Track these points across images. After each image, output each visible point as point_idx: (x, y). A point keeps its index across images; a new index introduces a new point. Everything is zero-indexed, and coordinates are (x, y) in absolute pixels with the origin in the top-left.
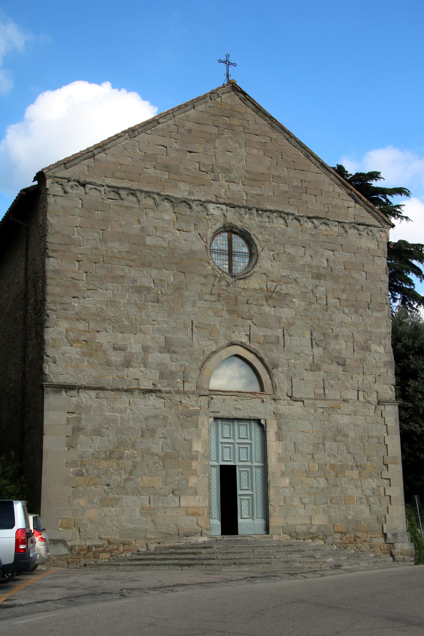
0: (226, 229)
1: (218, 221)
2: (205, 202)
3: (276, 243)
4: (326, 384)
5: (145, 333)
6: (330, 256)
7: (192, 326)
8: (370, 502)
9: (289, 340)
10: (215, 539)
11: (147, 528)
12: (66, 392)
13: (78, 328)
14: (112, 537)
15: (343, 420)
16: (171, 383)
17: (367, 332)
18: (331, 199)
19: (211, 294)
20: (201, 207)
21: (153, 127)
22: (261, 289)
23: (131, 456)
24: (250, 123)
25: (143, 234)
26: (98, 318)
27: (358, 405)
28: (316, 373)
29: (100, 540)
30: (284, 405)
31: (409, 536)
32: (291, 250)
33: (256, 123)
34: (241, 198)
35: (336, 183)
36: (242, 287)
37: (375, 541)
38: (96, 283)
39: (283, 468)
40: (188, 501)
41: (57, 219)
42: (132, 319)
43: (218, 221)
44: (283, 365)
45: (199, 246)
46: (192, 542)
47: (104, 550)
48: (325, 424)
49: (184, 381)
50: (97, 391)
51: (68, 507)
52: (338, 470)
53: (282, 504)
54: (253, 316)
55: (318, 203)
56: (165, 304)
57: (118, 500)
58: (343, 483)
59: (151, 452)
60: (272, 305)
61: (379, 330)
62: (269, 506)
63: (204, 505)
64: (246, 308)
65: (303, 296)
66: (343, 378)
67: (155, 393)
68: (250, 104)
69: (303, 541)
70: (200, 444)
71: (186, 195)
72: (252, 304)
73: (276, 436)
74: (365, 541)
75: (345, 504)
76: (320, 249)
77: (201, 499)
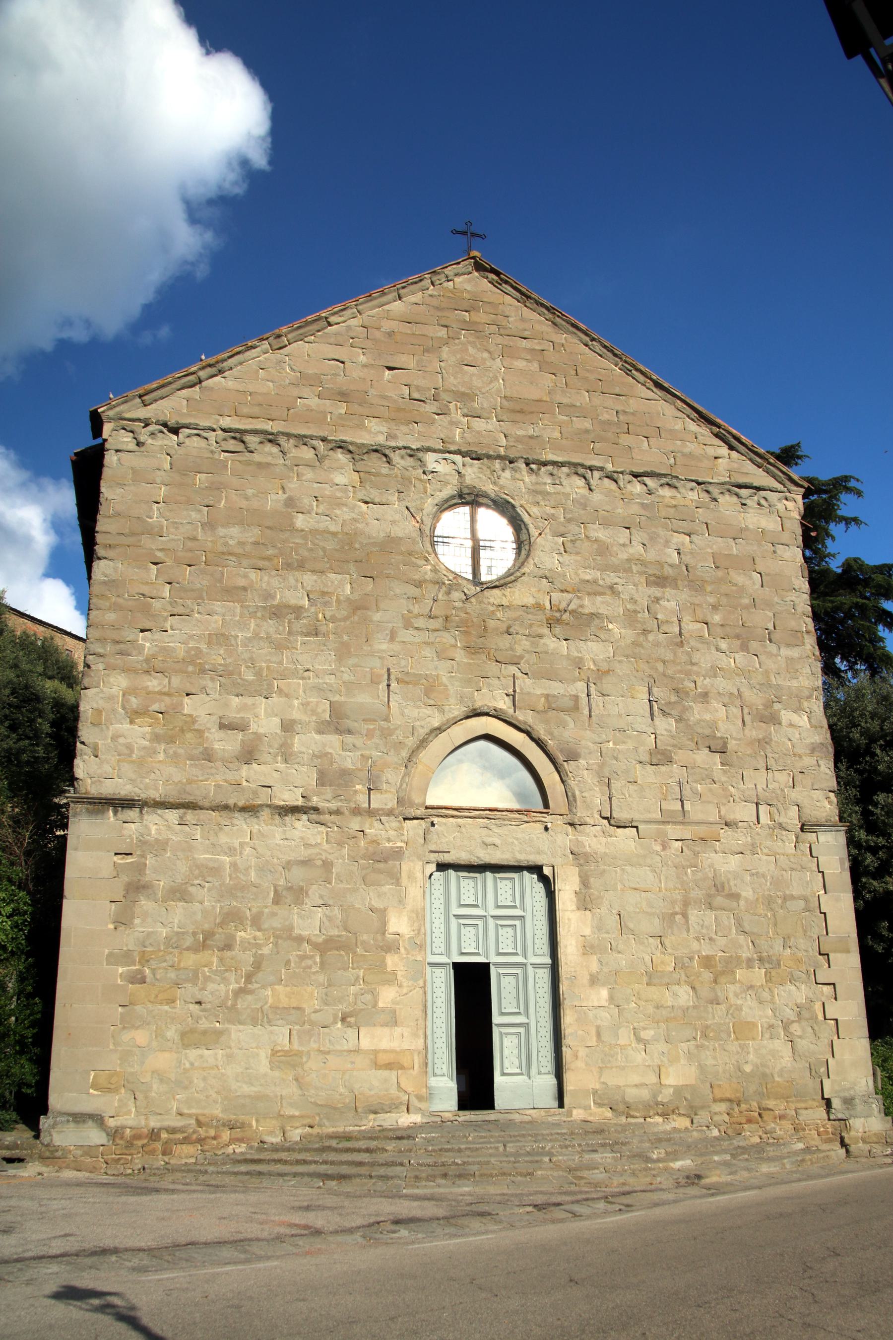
0: (464, 498)
1: (447, 483)
2: (418, 450)
3: (569, 520)
4: (687, 792)
5: (287, 696)
6: (683, 544)
7: (389, 679)
8: (791, 1033)
9: (601, 705)
10: (440, 1119)
11: (284, 1094)
12: (115, 813)
13: (148, 687)
14: (207, 1111)
15: (724, 863)
16: (340, 793)
17: (770, 686)
18: (679, 443)
19: (430, 617)
20: (412, 459)
21: (319, 331)
22: (539, 607)
23: (249, 943)
24: (511, 319)
25: (289, 510)
26: (190, 668)
27: (758, 834)
28: (663, 768)
29: (179, 1117)
30: (595, 836)
31: (881, 1102)
32: (599, 533)
33: (523, 319)
34: (495, 442)
35: (688, 416)
36: (496, 603)
37: (804, 1115)
38: (189, 602)
39: (594, 967)
40: (377, 1039)
41: (119, 491)
42: (261, 669)
43: (447, 483)
44: (590, 753)
45: (407, 528)
46: (386, 1125)
47: (185, 1138)
48: (686, 874)
49: (370, 789)
50: (182, 811)
51: (111, 1047)
52: (720, 969)
53: (593, 1042)
54: (521, 657)
55: (654, 450)
56: (332, 637)
57: (219, 1033)
58: (731, 995)
59: (294, 935)
60: (562, 637)
61: (795, 684)
62: (564, 1049)
63: (413, 1048)
64: (504, 642)
65: (630, 617)
66: (724, 779)
67: (305, 813)
68: (509, 288)
69: (642, 1120)
70: (406, 919)
71: (381, 439)
72: (517, 633)
73: (578, 900)
74: (782, 1117)
75: (737, 1039)
76: (662, 532)
77: (406, 1034)
